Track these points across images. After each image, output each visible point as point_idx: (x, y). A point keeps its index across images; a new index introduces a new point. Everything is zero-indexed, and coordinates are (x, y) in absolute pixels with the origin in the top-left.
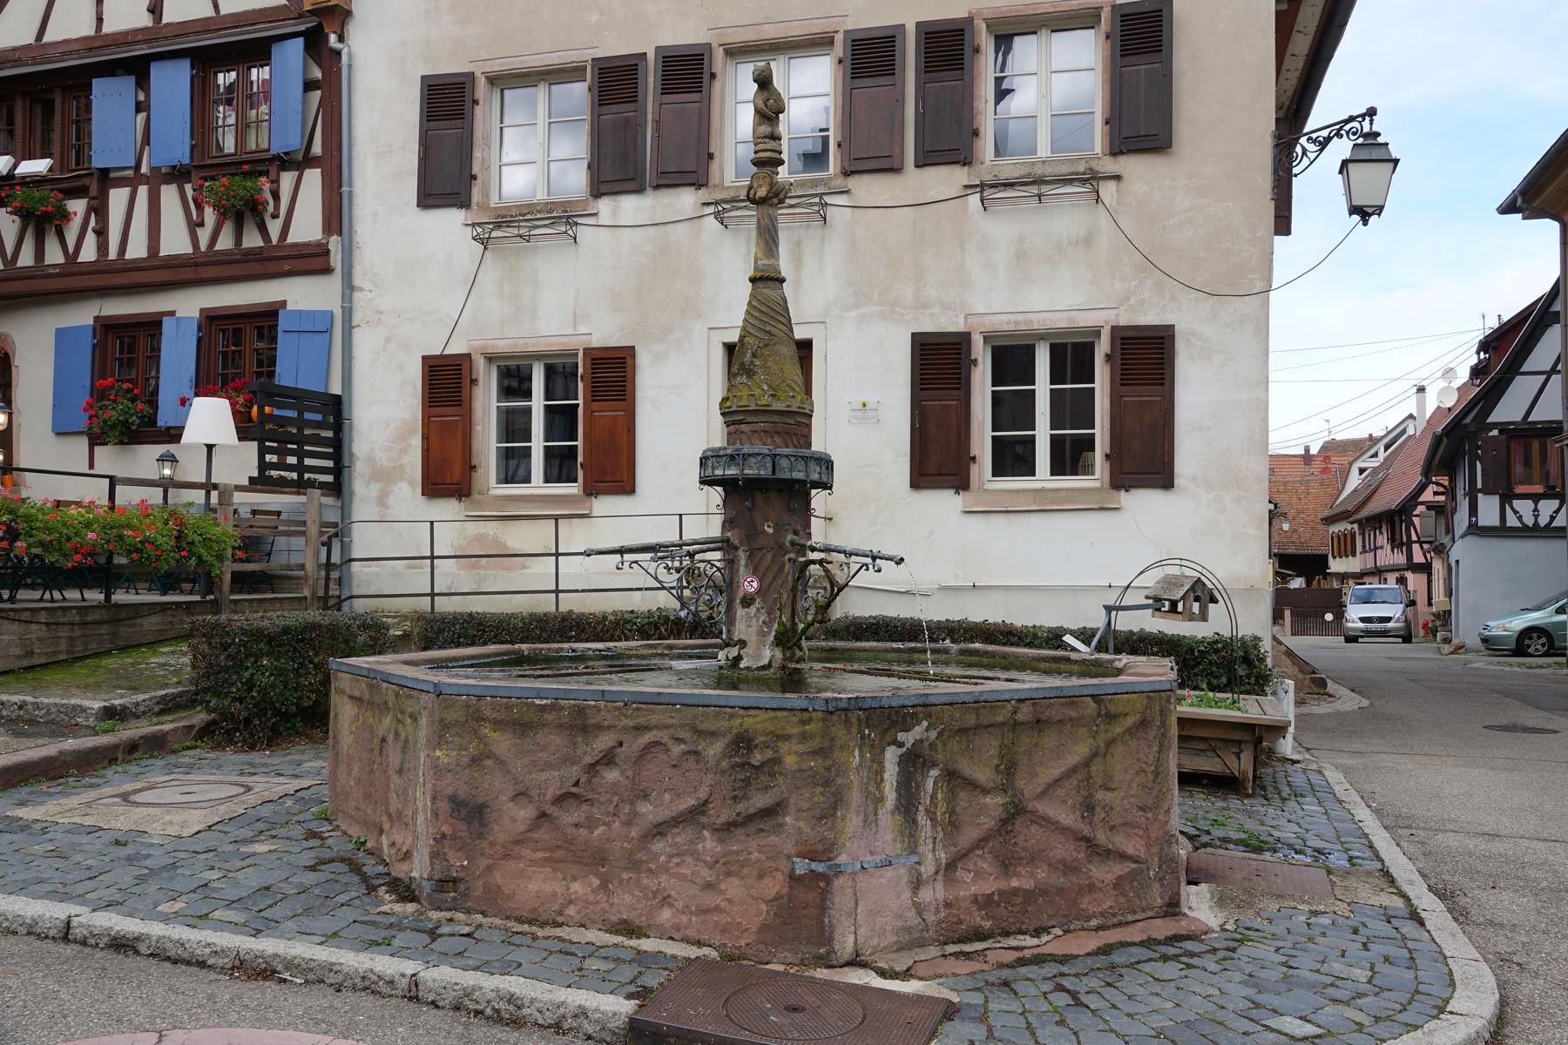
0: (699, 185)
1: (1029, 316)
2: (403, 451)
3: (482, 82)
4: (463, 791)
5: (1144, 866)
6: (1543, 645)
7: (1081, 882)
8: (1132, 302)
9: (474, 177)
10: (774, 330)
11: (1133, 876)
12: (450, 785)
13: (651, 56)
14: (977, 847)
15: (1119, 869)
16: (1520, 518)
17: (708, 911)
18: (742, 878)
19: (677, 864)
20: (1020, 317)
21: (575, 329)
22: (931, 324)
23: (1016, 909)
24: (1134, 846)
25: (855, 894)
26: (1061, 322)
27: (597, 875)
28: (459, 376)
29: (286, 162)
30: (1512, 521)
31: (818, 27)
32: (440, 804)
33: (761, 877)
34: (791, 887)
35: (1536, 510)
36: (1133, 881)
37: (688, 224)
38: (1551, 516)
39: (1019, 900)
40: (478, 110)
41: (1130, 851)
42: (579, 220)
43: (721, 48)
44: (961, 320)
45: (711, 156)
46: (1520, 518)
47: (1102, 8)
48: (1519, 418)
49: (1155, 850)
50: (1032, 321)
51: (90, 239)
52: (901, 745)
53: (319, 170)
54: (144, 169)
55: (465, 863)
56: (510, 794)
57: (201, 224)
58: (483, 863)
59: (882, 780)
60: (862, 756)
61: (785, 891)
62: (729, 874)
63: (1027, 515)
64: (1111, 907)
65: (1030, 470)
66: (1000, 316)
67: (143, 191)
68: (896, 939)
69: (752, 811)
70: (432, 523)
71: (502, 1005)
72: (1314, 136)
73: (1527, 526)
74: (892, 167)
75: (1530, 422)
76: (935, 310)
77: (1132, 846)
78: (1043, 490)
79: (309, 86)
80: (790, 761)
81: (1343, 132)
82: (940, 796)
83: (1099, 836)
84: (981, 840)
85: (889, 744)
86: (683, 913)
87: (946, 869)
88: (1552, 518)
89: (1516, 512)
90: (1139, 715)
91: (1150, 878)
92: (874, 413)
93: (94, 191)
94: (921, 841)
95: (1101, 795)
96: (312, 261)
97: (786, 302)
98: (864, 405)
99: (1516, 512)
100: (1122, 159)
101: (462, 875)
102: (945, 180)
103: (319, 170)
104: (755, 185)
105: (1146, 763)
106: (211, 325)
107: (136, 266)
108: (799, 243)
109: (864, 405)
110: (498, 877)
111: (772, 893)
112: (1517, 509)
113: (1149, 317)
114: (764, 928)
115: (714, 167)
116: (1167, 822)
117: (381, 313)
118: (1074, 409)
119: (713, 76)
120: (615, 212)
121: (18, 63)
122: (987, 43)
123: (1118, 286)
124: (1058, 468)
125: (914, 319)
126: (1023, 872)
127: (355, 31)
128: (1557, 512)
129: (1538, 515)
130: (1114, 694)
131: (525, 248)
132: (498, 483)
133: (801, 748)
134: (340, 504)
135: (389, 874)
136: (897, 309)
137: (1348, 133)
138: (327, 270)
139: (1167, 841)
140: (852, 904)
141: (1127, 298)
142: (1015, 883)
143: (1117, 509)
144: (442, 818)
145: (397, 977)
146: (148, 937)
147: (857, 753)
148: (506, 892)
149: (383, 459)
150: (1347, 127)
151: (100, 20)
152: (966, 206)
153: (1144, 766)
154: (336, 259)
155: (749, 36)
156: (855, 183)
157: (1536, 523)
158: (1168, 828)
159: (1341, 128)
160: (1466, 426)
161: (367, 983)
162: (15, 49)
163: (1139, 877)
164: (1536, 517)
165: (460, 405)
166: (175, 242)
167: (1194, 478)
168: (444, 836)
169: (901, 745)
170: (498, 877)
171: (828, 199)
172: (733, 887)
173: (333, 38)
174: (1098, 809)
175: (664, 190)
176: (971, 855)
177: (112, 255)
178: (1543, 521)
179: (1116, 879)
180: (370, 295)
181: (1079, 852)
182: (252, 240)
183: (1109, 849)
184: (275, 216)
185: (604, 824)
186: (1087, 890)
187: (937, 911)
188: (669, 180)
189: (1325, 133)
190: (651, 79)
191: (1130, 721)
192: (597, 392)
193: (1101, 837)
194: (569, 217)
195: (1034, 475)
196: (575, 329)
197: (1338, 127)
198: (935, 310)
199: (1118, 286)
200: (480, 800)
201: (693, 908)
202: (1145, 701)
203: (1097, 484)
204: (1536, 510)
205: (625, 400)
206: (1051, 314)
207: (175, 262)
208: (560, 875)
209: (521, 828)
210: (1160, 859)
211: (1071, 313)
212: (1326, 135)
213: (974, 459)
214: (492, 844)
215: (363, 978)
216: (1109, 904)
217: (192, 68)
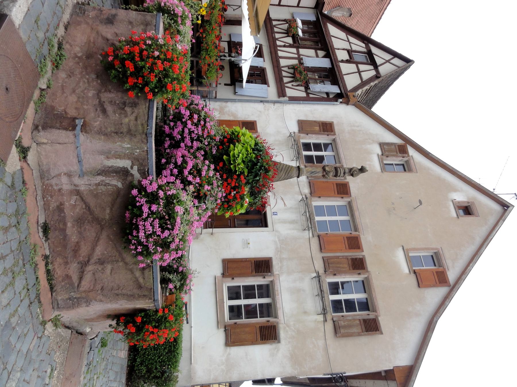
0: (311, 194)
1: (280, 294)
2: (229, 115)
3: (334, 137)
5: (76, 290)
7: (69, 258)
9: (307, 134)
10: (282, 171)
11: (72, 284)
14: (86, 206)
15: (75, 278)
17: (63, 89)
18: (76, 102)
19: (84, 82)
20: (279, 292)
23: (57, 224)
24: (85, 285)
25: (65, 143)
26: (279, 305)
29: (307, 88)
31: (360, 227)
33: (76, 108)
34: (71, 118)
36: (69, 284)
37: (300, 191)
39: (61, 226)
40: (326, 136)
41: (83, 283)
42: (298, 161)
43: (350, 200)
44: (277, 273)
45: (320, 197)
47: (376, 312)
49: (83, 295)
51: (283, 44)
52: (132, 168)
53: (306, 96)
54: (301, 56)
55: (90, 17)
56: (117, 32)
57: (289, 68)
58: (90, 22)
59: (117, 158)
60: (128, 148)
61: (69, 116)
62: (79, 98)
63: (215, 298)
64: (57, 273)
65: (230, 298)
66: (279, 285)
67: (296, 56)
68: (45, 164)
69: (105, 106)
76: (280, 264)
77: (86, 284)
78: (224, 302)
79: (327, 94)
80: (126, 120)
82: (109, 187)
83: (90, 267)
84: (89, 208)
85: (132, 162)
86: (63, 81)
87: (76, 190)
90: (143, 284)
91: (70, 293)
93: (295, 45)
94: (89, 178)
95: (109, 267)
96: (281, 93)
97: (291, 178)
98: (249, 244)
101: (86, 15)
102: (319, 266)
103: (306, 96)
104: (329, 167)
105: (123, 289)
106: (261, 70)
107: (276, 54)
108: (297, 223)
109: (249, 244)
110: (84, 26)
111: (68, 111)
113: (282, 334)
114: (53, 108)
115: (317, 199)
116: (96, 300)
117: (268, 110)
118: (251, 312)
119: (342, 198)
121: (326, 31)
122: (360, 278)
123: (292, 323)
124: (232, 308)
126: (74, 229)
127: (344, 106)
130: (153, 272)
131: (289, 147)
133: (132, 124)
134: (213, 98)
135: (124, 350)
136: (279, 253)
138: (279, 96)
139: (87, 301)
140: (61, 141)
141: (288, 326)
142: (69, 225)
143: (218, 328)
147: (129, 146)
148: (77, 27)
149: (226, 110)
151: (338, 49)
152: (312, 273)
153: (122, 288)
154: (282, 99)
155: (355, 207)
156: (316, 239)
158: (93, 301)
162: (329, 31)
163: (71, 287)
166: (283, 62)
167: (229, 354)
168: (102, 11)
169: (132, 168)
170: (84, 26)
171: (311, 231)
172: (73, 98)
173: (341, 100)
174: (102, 266)
175: (309, 184)
176: (82, 203)
177: (279, 48)
179: (70, 276)
180: (273, 108)
181: (83, 257)
182: (286, 80)
183: (84, 272)
184: (292, 85)
186: (66, 261)
187: (57, 185)
191: (141, 280)
193: (90, 268)
194: (299, 158)
195: (228, 300)
198: (280, 264)
199: (292, 323)
201: (64, 84)
202: (149, 287)
203: (226, 321)
206: (281, 302)
207: (278, 62)
210: (79, 298)
211: (282, 308)
213: (233, 279)
214: (98, 25)
216: (59, 272)
217: (329, 68)
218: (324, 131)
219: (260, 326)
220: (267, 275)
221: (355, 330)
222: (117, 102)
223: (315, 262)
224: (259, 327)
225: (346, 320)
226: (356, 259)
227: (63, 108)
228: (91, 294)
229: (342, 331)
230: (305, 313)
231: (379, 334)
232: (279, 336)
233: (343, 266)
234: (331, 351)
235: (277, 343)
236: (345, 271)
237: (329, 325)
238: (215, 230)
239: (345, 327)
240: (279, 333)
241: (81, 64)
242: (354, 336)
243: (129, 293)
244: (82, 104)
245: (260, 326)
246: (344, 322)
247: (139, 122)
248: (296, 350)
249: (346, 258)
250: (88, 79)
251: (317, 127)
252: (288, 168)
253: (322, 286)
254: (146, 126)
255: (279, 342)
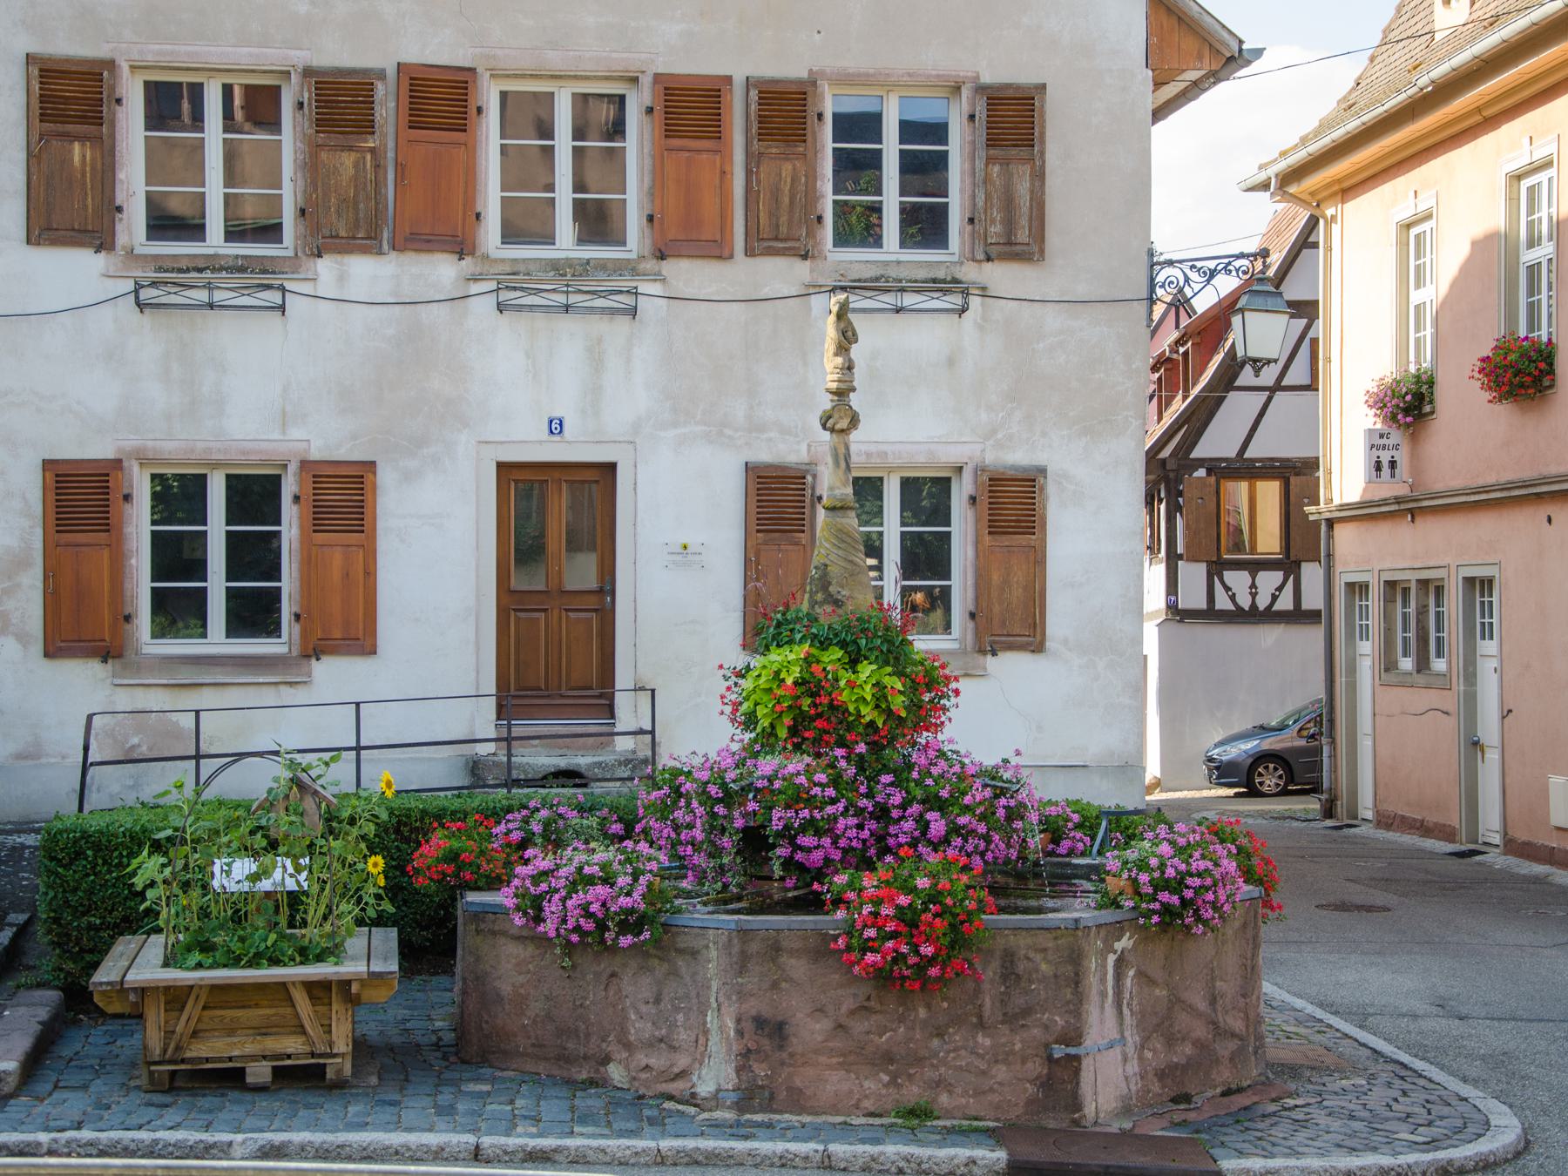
4: (767, 1012)
6: (1278, 785)
8: (1000, 436)
12: (753, 1006)
13: (391, 72)
16: (1233, 598)
19: (954, 1058)
20: (873, 448)
21: (284, 433)
22: (765, 455)
27: (887, 1072)
28: (106, 490)
30: (1222, 602)
32: (743, 1024)
33: (1024, 1062)
35: (1253, 586)
38: (1273, 595)
39: (1178, 1073)
44: (804, 448)
46: (1233, 598)
48: (1232, 454)
50: (886, 453)
62: (996, 1062)
70: (197, 712)
71: (902, 1164)
72: (1199, 264)
73: (1243, 609)
74: (718, 250)
75: (1247, 460)
76: (772, 435)
81: (1230, 267)
88: (1274, 598)
89: (1227, 589)
92: (697, 558)
98: (685, 547)
99: (1227, 589)
100: (988, 267)
108: (600, 340)
112: (1250, 598)
113: (1017, 457)
120: (342, 278)
123: (984, 416)
125: (746, 444)
128: (1280, 589)
129: (1256, 593)
132: (153, 637)
137: (1237, 270)
141: (994, 432)
144: (747, 1036)
145: (811, 1154)
146: (567, 1148)
150: (1238, 263)
156: (670, 267)
157: (1254, 605)
159: (1229, 263)
160: (1164, 461)
161: (784, 1161)
164: (1254, 595)
165: (108, 531)
167: (1065, 642)
168: (749, 1050)
172: (1001, 1073)
178: (1263, 602)
185: (892, 1030)
188: (417, 240)
189: (1212, 264)
190: (387, 107)
192: (320, 519)
196: (284, 433)
197: (1226, 261)
198: (772, 435)
200: (780, 1018)
204: (1253, 586)
205: (363, 532)
208: (853, 1076)
209: (820, 1038)
212: (1213, 267)
215: (781, 1158)
218: (98, 120)
219: (990, 533)
220: (813, 489)
221: (1023, 188)
222: (1003, 989)
223: (766, 292)
224: (991, 537)
225: (985, 212)
226: (762, 119)
227: (1028, 1085)
228: (1252, 1015)
229: (1022, 235)
230: (951, 362)
231: (1043, 101)
232: (1025, 469)
233: (789, 180)
234: (1082, 290)
235: (1045, 477)
236: (806, 176)
237: (1000, 275)
238: (623, 677)
239: (1010, 224)
240: (1013, 467)
241: (912, 1071)
242: (1043, 193)
243: (1251, 946)
244: (1012, 1052)
245: (990, 533)
246: (993, 221)
247: (1050, 945)
248: (1071, 414)
249: (753, 161)
250: (948, 1052)
251: (71, 151)
252: (844, 542)
253: (859, 281)
254: (1059, 932)
255: (1042, 471)
